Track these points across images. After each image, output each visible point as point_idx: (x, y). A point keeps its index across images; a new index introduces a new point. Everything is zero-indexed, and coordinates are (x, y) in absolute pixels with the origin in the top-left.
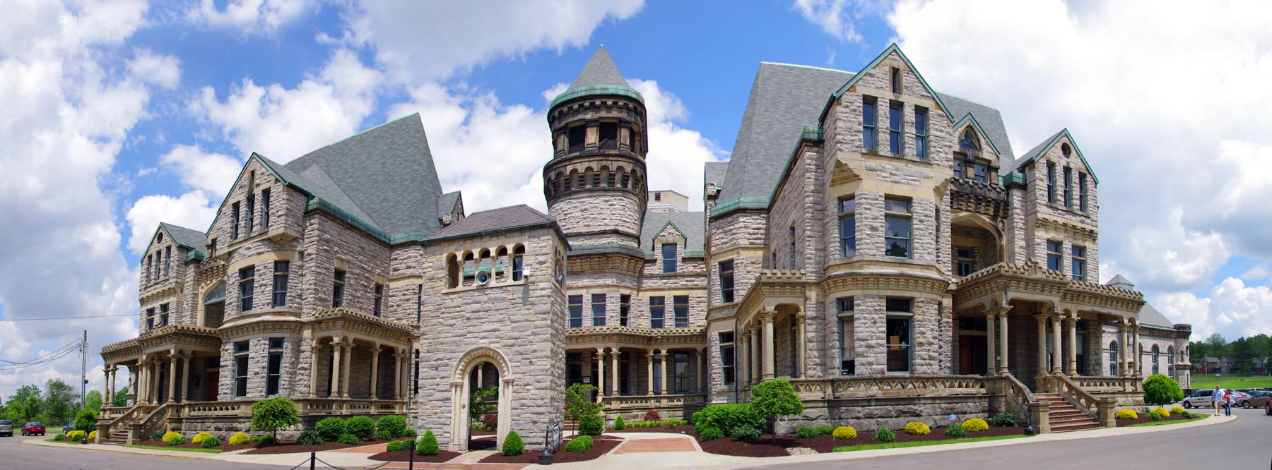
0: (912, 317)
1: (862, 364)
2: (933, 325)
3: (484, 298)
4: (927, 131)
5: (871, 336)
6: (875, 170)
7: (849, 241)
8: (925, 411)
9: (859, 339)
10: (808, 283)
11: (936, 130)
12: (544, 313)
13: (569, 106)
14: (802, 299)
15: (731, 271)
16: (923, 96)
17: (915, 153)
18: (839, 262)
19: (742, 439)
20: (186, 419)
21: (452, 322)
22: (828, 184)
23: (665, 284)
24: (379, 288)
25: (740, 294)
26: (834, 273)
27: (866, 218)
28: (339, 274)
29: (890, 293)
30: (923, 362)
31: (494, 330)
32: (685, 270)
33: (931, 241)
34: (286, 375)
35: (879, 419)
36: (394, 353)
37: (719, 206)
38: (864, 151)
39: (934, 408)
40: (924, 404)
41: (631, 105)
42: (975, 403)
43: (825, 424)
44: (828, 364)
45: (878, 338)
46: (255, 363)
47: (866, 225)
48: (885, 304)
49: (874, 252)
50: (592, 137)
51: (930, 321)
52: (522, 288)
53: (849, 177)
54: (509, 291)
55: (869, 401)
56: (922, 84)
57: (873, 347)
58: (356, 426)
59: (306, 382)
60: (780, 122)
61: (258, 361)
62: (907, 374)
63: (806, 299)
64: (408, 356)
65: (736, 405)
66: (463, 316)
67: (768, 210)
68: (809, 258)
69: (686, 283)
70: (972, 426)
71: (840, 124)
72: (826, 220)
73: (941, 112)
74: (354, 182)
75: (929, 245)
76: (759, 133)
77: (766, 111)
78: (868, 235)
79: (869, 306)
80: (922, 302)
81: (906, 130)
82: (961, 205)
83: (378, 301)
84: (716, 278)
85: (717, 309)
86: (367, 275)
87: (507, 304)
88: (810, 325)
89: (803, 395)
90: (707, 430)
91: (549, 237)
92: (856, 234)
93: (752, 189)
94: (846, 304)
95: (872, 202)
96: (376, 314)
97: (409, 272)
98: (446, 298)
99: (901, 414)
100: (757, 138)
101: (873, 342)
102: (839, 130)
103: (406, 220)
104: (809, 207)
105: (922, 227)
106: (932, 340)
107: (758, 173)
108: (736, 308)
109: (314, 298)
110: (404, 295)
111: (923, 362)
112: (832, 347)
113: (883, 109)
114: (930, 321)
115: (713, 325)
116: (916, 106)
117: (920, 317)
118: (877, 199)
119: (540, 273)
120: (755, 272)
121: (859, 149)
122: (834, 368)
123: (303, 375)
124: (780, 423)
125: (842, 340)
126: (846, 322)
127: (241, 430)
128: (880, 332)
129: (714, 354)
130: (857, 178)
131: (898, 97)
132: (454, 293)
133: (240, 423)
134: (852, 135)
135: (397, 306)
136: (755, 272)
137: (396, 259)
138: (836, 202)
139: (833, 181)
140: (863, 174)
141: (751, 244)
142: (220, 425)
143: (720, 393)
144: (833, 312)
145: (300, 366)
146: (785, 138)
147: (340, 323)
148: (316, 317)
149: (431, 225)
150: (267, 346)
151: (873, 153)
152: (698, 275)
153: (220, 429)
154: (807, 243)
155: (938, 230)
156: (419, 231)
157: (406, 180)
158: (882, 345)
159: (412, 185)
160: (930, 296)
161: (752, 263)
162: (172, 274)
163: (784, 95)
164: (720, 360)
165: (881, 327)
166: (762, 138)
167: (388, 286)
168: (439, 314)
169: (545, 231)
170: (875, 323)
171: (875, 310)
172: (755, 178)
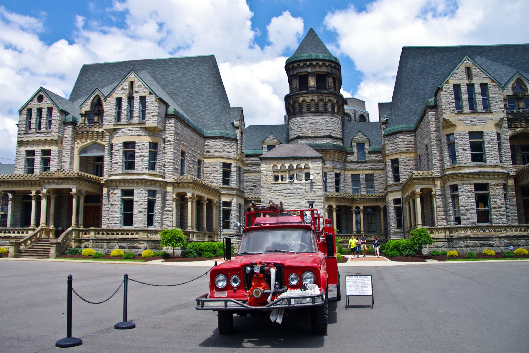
0: (489, 193)
1: (464, 219)
2: (501, 197)
3: (292, 187)
4: (488, 95)
5: (468, 205)
6: (462, 121)
7: (453, 158)
8: (495, 244)
9: (462, 206)
10: (436, 177)
11: (493, 94)
12: (320, 196)
13: (298, 63)
14: (433, 186)
15: (397, 165)
16: (484, 78)
17: (482, 108)
18: (449, 167)
19: (407, 256)
20: (93, 240)
21: (277, 197)
22: (441, 128)
23: (359, 167)
24: (199, 162)
25: (403, 178)
26: (447, 173)
27: (460, 145)
28: (183, 153)
29: (475, 182)
30: (497, 217)
31: (297, 203)
32: (371, 159)
33: (495, 153)
34: (158, 214)
35: (472, 248)
36: (211, 203)
37: (388, 129)
38: (456, 112)
39: (501, 243)
40: (495, 240)
41: (333, 65)
42: (526, 240)
43: (446, 250)
44: (449, 219)
45: (472, 205)
46: (139, 205)
47: (460, 149)
48: (473, 187)
49: (465, 161)
50: (312, 82)
51: (499, 195)
52: (309, 184)
53: (450, 125)
54: (303, 185)
55: (466, 238)
56: (482, 71)
57: (469, 210)
58: (209, 248)
59: (171, 220)
60: (416, 81)
61: (141, 204)
62: (488, 224)
63: (435, 185)
64: (219, 205)
65: (404, 240)
66: (282, 195)
67: (414, 131)
68: (435, 165)
69: (371, 166)
70: (519, 252)
71: (443, 100)
72: (442, 146)
73: (494, 84)
74: (175, 89)
75: (494, 155)
76: (406, 88)
77: (408, 75)
78: (462, 153)
79: (465, 189)
80: (493, 185)
81: (477, 98)
82: (517, 125)
83: (199, 169)
84: (389, 168)
85: (391, 185)
86: (194, 154)
87: (303, 191)
88: (438, 198)
89: (436, 235)
90: (390, 253)
91: (320, 162)
92: (456, 153)
93: (405, 120)
94: (454, 188)
95: (462, 136)
96: (199, 176)
97: (217, 154)
98: (274, 186)
99: (482, 245)
100: (405, 91)
101: (469, 208)
102: (443, 103)
103: (213, 121)
104: (433, 139)
105: (490, 146)
106: (501, 205)
107: (407, 110)
108: (401, 186)
109: (173, 168)
110: (214, 168)
111: (497, 217)
112: (449, 210)
113: (464, 89)
114: (499, 195)
115: (389, 194)
116: (481, 84)
117: (493, 193)
118: (465, 135)
119: (317, 178)
120: (410, 165)
121: (454, 111)
122: (451, 221)
123: (168, 214)
124: (425, 249)
125: (454, 207)
126: (455, 198)
127: (141, 248)
128: (472, 202)
129: (391, 211)
130: (454, 126)
131: (471, 81)
132: (277, 184)
133: (140, 244)
134: (449, 105)
135: (210, 174)
136: (410, 165)
137: (208, 145)
138: (445, 137)
139: (443, 127)
140: (457, 123)
141: (407, 150)
142: (124, 245)
143: (396, 233)
144: (448, 192)
145: (166, 209)
146: (420, 90)
147: (191, 185)
148: (176, 180)
149: (228, 126)
150: (147, 195)
151: (461, 113)
152: (379, 162)
153: (124, 248)
154: (434, 157)
155: (499, 144)
156: (222, 130)
157: (211, 96)
158: (473, 209)
159: (214, 100)
160: (497, 181)
161: (409, 160)
162: (55, 128)
163: (418, 65)
164: (394, 215)
165: (472, 199)
166: (408, 90)
167: (203, 161)
168: (270, 193)
169: (319, 160)
170: (469, 198)
171: (469, 191)
172: (406, 113)
